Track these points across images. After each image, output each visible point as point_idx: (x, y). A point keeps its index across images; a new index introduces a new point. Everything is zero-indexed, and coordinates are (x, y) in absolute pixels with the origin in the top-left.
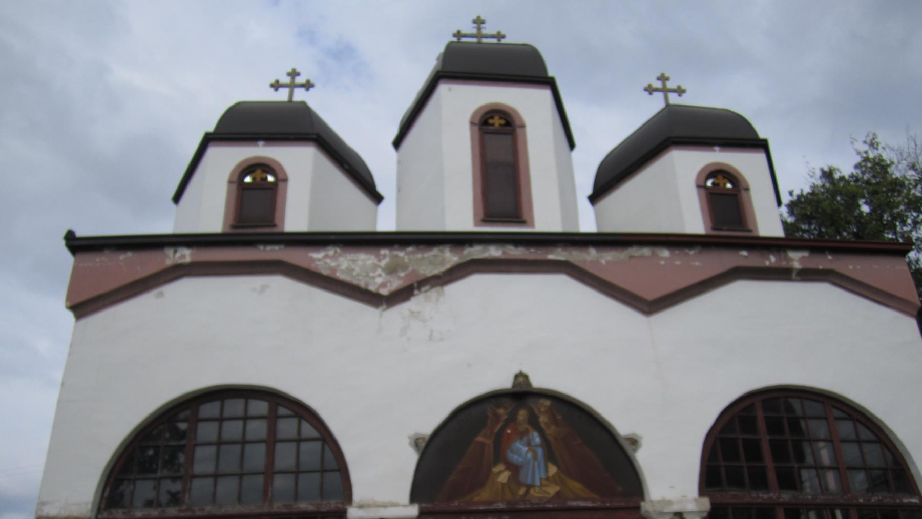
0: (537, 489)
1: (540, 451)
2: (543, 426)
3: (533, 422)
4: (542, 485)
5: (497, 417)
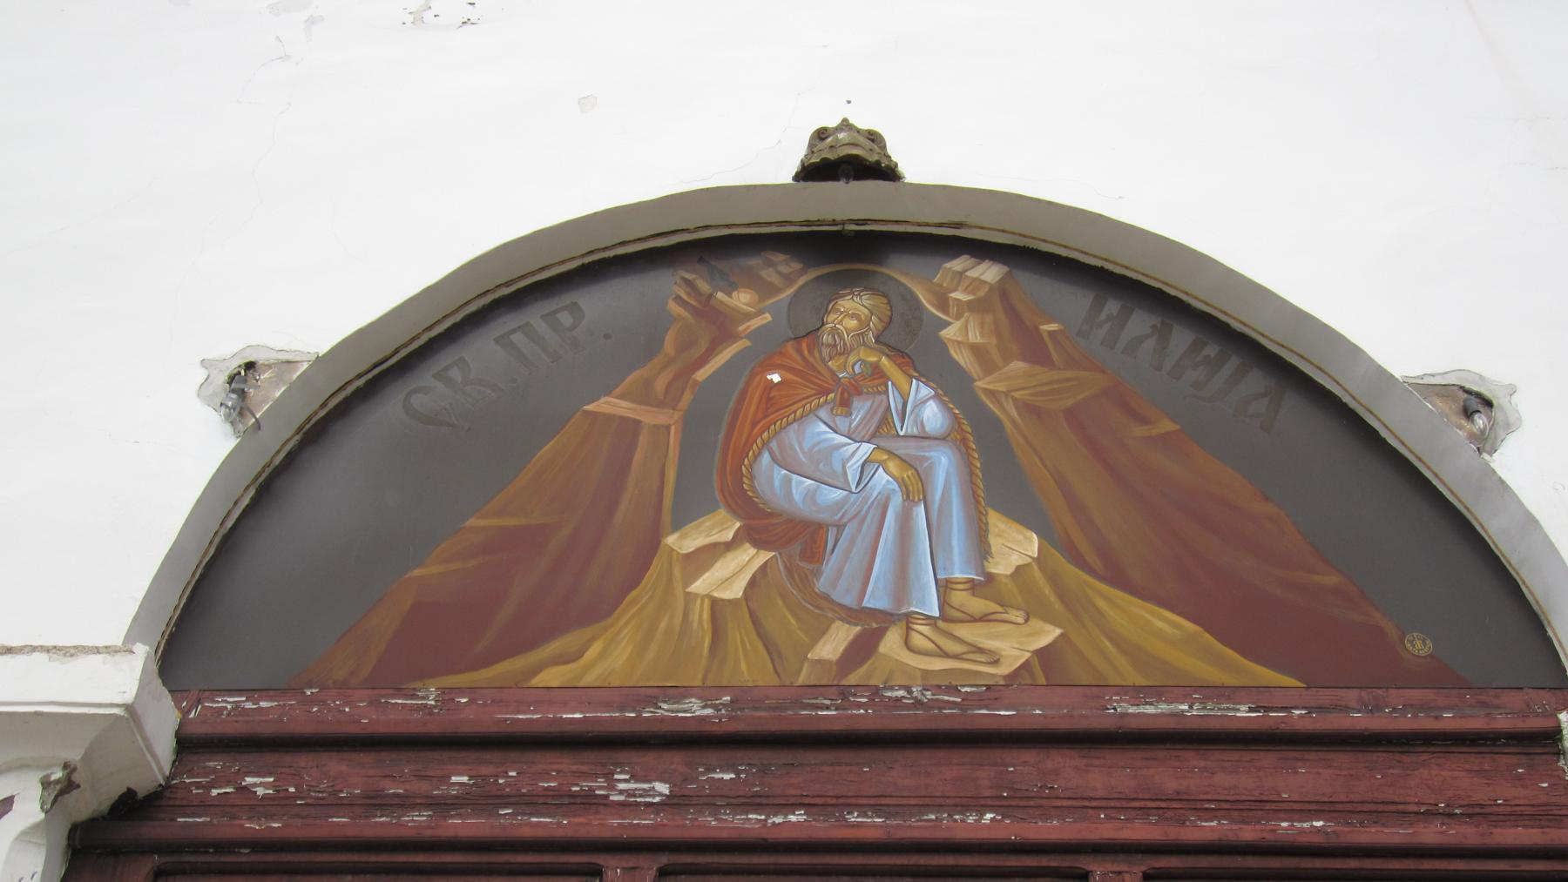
0: (922, 635)
1: (943, 464)
2: (963, 358)
4: (948, 615)
5: (721, 326)
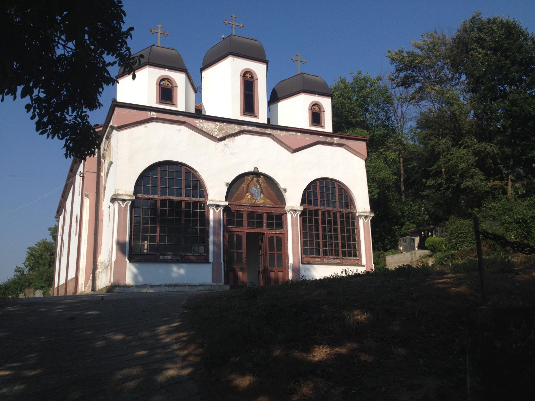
3: (258, 181)
